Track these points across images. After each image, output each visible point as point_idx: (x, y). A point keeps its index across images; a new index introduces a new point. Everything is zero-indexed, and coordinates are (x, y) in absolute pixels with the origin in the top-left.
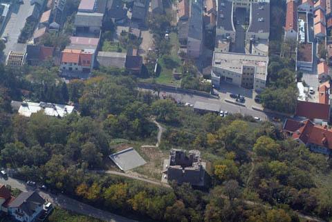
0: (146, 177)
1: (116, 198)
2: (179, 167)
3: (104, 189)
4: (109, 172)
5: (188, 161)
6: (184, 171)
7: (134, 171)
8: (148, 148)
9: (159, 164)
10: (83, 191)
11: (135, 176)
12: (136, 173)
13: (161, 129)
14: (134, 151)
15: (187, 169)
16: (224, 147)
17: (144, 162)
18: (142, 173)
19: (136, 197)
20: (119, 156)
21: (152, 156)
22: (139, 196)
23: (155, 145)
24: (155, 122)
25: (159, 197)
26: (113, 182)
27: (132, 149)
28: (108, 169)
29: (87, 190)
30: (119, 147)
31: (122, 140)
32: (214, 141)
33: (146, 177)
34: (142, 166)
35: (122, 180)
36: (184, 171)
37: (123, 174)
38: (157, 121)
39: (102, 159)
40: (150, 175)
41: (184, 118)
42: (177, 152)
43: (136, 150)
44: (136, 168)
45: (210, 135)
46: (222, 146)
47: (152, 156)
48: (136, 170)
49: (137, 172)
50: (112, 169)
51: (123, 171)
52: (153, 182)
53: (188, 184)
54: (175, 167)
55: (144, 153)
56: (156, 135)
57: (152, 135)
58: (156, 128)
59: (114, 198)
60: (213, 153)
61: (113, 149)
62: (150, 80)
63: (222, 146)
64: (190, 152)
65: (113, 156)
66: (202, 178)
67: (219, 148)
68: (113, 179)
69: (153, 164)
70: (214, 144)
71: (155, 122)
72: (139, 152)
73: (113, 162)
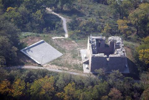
0: (67, 69)
1: (44, 93)
2: (102, 55)
3: (28, 84)
4: (26, 67)
5: (110, 49)
6: (108, 59)
7: (52, 64)
8: (60, 40)
9: (76, 55)
10: (5, 88)
11: (54, 68)
12: (54, 66)
13: (65, 20)
14: (46, 43)
15: (111, 56)
16: (136, 33)
17: (59, 54)
18: (61, 65)
19: (66, 89)
20: (31, 49)
21: (67, 47)
22: (69, 88)
23: (64, 36)
24: (53, 13)
25: (90, 87)
26: (36, 76)
27: (43, 42)
28: (23, 64)
29: (10, 87)
30: (28, 40)
31: (29, 34)
32: (126, 27)
33: (67, 69)
34: (59, 59)
35: (44, 73)
36: (108, 59)
37: (40, 68)
38: (55, 12)
39: (16, 53)
40: (69, 66)
41: (81, 8)
42: (97, 40)
43: (47, 42)
44: (53, 61)
45: (120, 21)
46: (133, 32)
47: (67, 47)
48: (54, 62)
49: (56, 64)
50: (28, 64)
51: (40, 65)
52: (75, 73)
53: (117, 71)
54: (98, 55)
55: (57, 45)
56: (61, 26)
57: (56, 26)
58: (60, 19)
59: (43, 92)
60: (126, 40)
61: (23, 43)
62: (63, 67)
63: (133, 32)
64: (110, 38)
65: (25, 50)
66: (126, 66)
67: (130, 34)
68: (35, 73)
69: (69, 55)
70: (125, 30)
71: (53, 13)
72: (51, 44)
73: (29, 59)
